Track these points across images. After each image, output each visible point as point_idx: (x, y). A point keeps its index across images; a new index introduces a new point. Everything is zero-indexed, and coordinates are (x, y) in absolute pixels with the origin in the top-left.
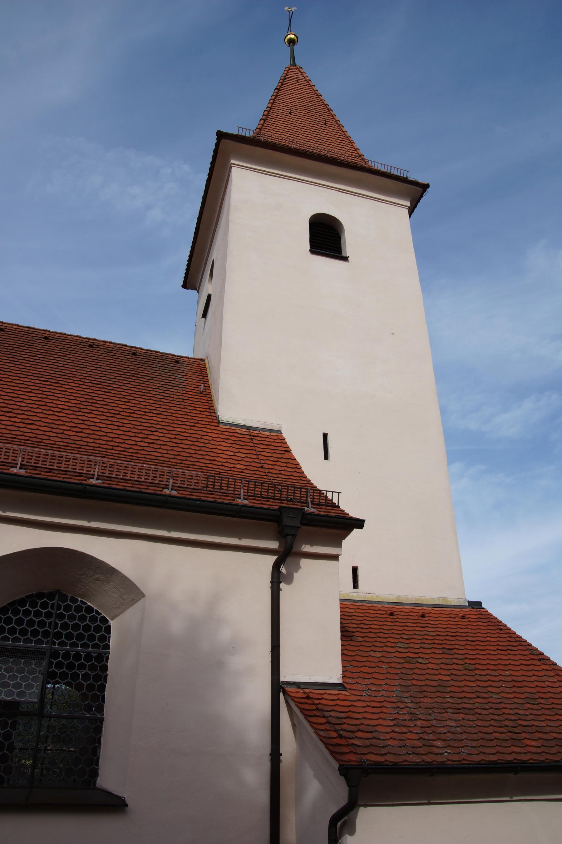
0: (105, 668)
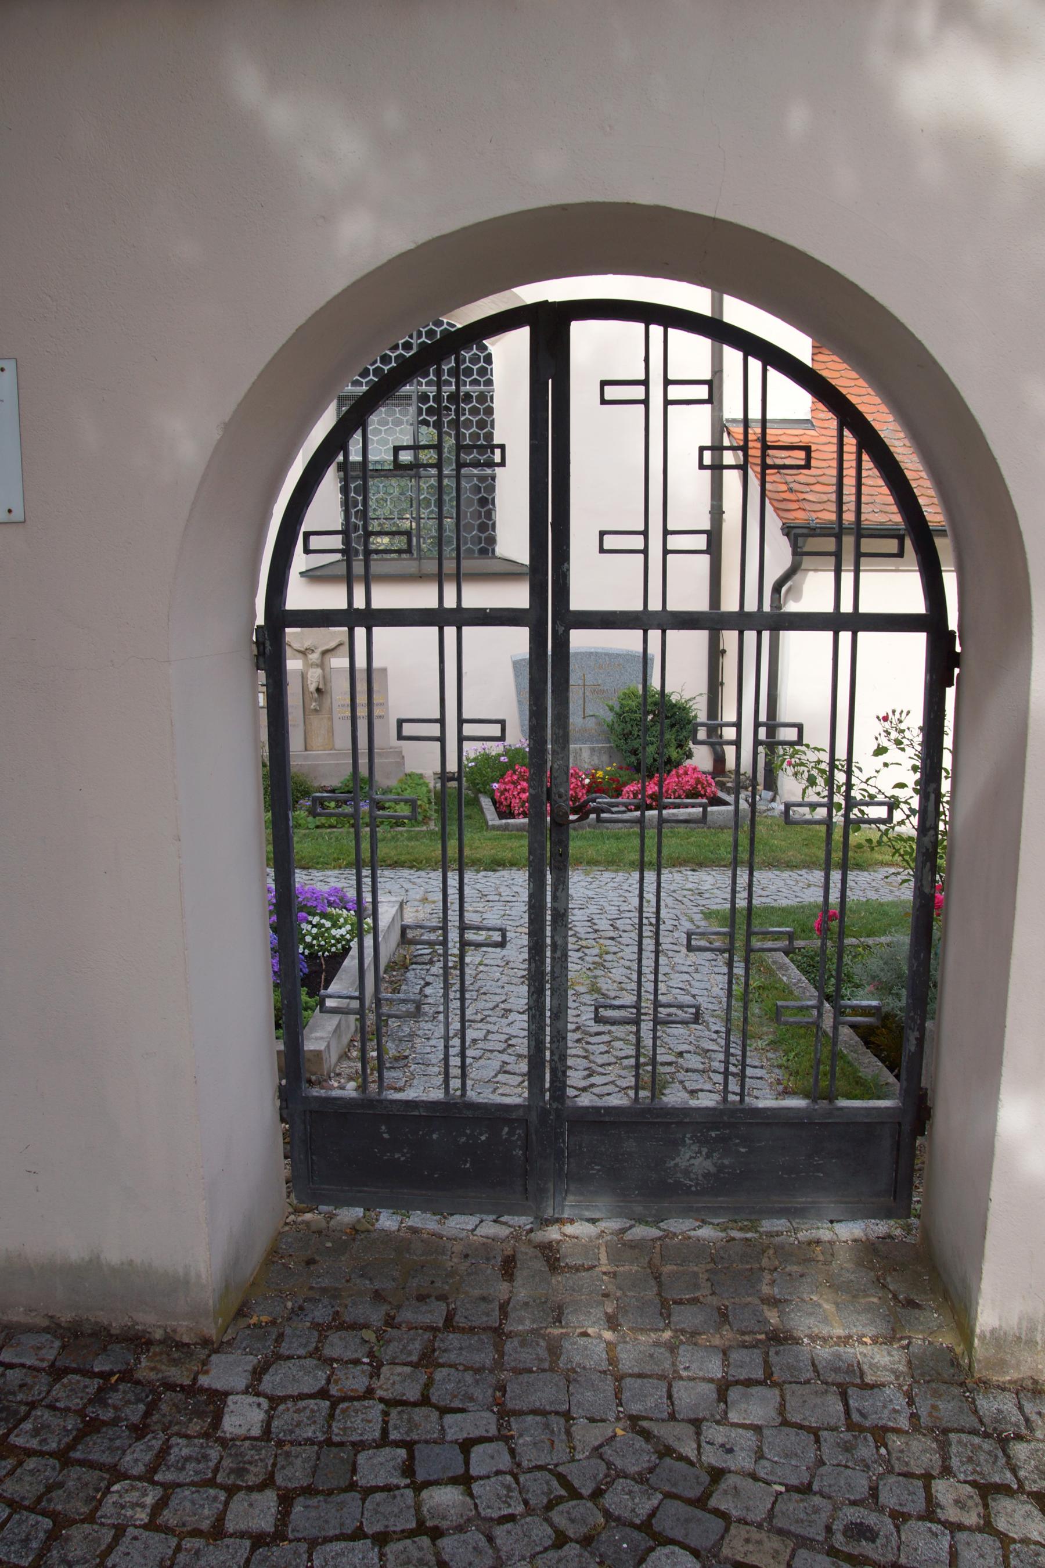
0: (490, 411)
